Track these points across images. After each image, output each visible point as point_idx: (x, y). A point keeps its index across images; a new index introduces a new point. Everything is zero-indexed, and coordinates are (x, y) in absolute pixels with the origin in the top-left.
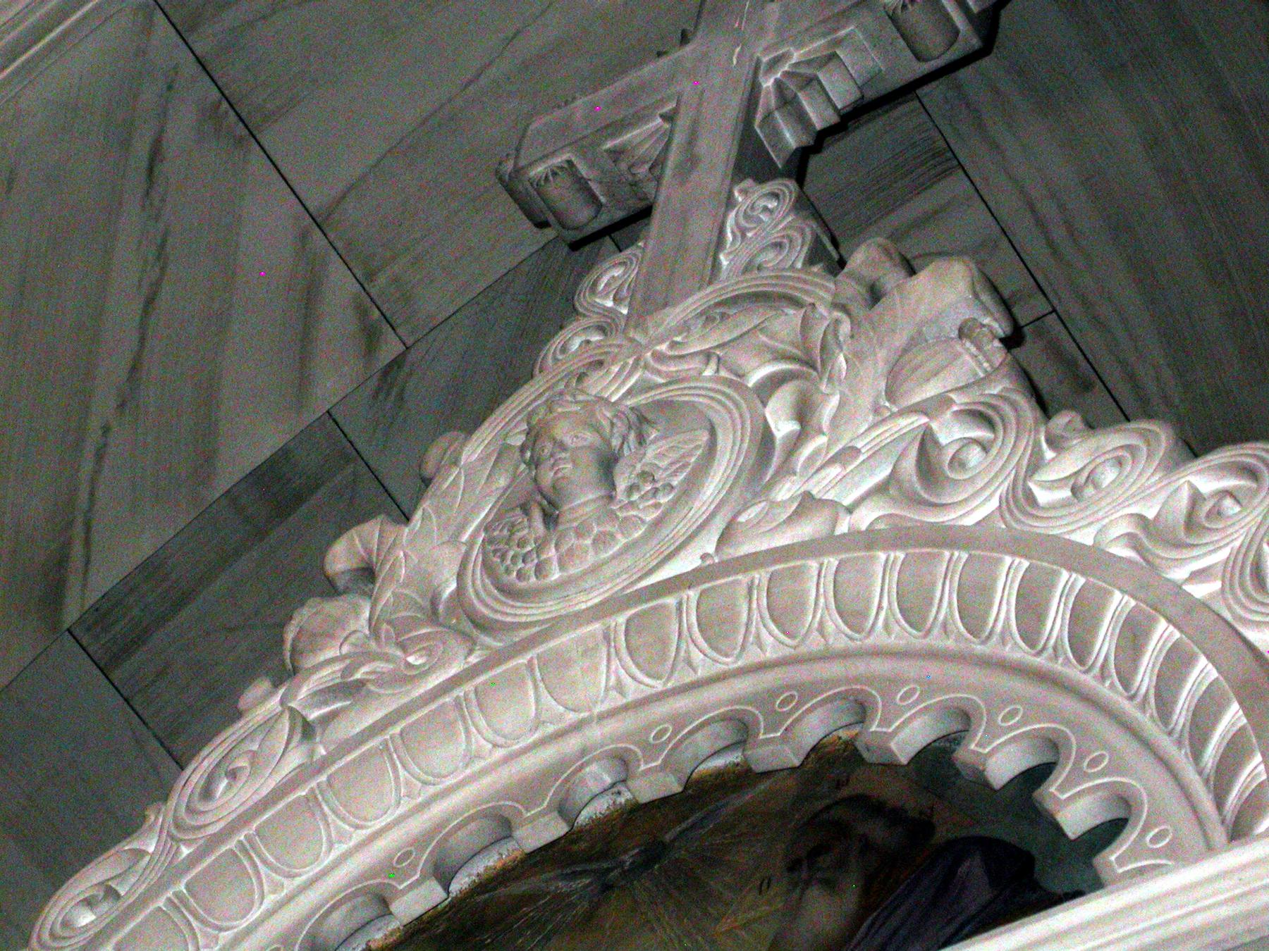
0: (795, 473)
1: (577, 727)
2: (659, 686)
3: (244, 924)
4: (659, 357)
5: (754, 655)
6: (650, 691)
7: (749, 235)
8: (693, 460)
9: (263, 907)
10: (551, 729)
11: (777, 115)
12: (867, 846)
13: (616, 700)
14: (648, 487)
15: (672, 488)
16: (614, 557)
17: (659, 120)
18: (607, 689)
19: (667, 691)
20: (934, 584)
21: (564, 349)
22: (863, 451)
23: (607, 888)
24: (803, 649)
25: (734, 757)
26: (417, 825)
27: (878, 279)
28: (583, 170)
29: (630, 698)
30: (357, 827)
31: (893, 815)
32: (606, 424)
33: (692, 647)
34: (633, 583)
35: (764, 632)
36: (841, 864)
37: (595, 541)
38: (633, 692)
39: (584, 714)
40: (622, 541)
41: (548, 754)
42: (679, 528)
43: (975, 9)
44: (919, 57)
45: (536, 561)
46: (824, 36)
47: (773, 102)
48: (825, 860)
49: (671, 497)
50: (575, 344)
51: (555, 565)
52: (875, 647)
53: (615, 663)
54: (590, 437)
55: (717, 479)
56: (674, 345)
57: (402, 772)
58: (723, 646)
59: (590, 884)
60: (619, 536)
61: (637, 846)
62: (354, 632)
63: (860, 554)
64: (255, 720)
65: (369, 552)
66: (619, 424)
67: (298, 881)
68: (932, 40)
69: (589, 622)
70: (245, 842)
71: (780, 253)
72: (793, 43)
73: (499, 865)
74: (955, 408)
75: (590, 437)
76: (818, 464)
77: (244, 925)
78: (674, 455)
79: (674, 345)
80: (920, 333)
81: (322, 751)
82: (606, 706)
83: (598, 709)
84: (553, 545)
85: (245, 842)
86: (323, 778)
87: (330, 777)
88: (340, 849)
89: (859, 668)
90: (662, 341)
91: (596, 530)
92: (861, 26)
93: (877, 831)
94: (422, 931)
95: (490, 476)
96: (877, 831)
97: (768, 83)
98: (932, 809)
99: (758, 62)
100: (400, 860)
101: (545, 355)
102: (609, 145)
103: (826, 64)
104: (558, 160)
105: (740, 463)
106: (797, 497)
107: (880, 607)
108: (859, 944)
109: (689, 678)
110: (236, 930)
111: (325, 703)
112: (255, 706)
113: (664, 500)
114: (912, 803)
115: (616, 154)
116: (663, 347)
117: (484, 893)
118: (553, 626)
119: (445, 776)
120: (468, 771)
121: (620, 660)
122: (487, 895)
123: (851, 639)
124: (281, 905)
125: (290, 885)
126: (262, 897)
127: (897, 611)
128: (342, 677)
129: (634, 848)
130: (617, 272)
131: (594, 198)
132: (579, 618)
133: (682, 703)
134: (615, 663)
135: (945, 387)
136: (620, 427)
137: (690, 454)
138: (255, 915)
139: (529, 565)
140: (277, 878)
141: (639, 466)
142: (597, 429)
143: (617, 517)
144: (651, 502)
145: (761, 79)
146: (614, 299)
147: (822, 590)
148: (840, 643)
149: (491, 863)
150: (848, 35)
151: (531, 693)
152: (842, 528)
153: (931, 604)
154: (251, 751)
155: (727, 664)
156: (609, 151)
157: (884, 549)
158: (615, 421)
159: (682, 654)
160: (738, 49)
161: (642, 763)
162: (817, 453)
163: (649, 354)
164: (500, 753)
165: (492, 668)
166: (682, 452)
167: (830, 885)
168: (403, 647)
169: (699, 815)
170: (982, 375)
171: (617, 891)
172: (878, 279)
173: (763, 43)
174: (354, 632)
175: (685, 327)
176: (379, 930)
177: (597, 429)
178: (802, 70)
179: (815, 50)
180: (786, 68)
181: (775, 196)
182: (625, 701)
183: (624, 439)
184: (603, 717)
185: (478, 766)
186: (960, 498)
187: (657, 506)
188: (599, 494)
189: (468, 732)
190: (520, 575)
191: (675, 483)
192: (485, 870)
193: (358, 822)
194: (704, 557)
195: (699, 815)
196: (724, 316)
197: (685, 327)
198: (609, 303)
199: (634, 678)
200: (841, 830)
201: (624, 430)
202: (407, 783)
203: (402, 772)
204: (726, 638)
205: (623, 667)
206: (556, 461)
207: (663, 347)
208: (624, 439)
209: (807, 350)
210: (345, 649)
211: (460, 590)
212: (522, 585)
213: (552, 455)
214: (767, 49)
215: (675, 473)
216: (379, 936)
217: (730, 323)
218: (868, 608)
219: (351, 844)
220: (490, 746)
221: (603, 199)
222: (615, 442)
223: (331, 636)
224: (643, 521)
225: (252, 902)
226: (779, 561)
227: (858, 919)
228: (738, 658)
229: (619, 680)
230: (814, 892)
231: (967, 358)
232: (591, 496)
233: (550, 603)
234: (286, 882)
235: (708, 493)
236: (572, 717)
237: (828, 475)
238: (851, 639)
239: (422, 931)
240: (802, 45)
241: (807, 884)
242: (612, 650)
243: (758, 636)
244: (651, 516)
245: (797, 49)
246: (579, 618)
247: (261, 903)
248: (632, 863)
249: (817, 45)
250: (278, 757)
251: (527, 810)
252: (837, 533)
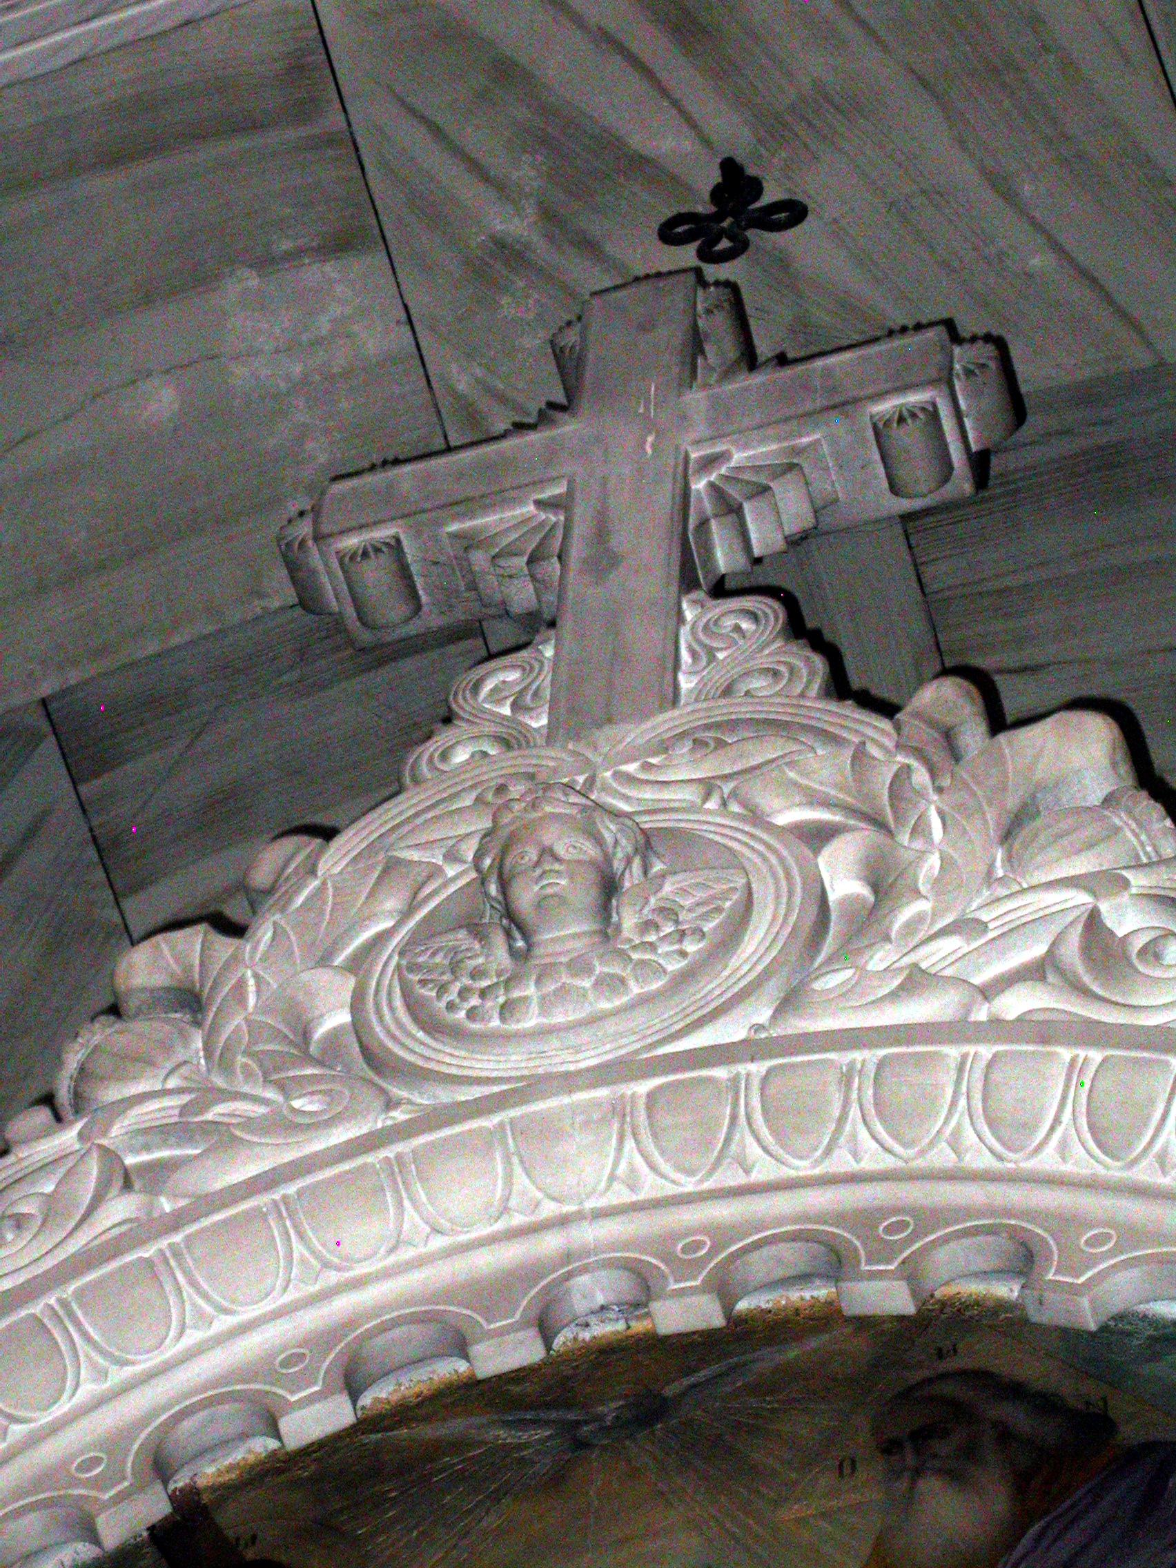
0: (887, 938)
1: (563, 1221)
2: (689, 1185)
3: (45, 1419)
4: (630, 779)
5: (842, 1162)
6: (672, 1190)
7: (721, 656)
8: (728, 904)
9: (75, 1400)
10: (518, 1220)
11: (714, 525)
12: (1005, 1435)
13: (621, 1195)
14: (668, 928)
15: (703, 935)
16: (616, 1012)
17: (530, 508)
18: (612, 1177)
19: (700, 1193)
20: (1151, 1101)
21: (445, 756)
22: (991, 926)
23: (581, 1445)
24: (920, 1163)
25: (821, 1292)
26: (311, 1320)
27: (953, 728)
28: (411, 551)
29: (641, 1196)
30: (227, 1311)
31: (1046, 1404)
32: (609, 839)
33: (750, 1140)
34: (653, 1046)
35: (863, 1134)
36: (969, 1452)
37: (596, 984)
38: (652, 1187)
39: (570, 1208)
40: (635, 989)
41: (512, 1254)
42: (713, 987)
43: (974, 447)
44: (895, 489)
45: (501, 1000)
46: (780, 440)
47: (708, 507)
48: (944, 1448)
49: (701, 945)
50: (461, 756)
51: (534, 1007)
52: (1032, 1171)
53: (630, 1144)
54: (590, 850)
55: (761, 933)
56: (647, 767)
57: (298, 1248)
58: (799, 1143)
59: (549, 1437)
60: (632, 983)
61: (621, 1397)
62: (185, 1062)
63: (1031, 1048)
64: (31, 1160)
65: (188, 969)
66: (624, 842)
67: (129, 1371)
68: (918, 472)
69: (592, 1086)
70: (58, 1308)
71: (776, 683)
72: (735, 443)
73: (395, 1398)
74: (1134, 891)
75: (590, 850)
76: (922, 935)
77: (43, 1421)
78: (701, 895)
79: (647, 767)
80: (1034, 797)
81: (166, 1205)
82: (601, 1203)
83: (591, 1204)
84: (534, 977)
85: (58, 1308)
86: (178, 1238)
87: (188, 1239)
88: (193, 1337)
89: (1014, 1196)
90: (628, 760)
91: (597, 972)
92: (834, 440)
93: (1019, 1417)
94: (280, 1471)
95: (371, 895)
96: (1019, 1417)
97: (699, 485)
98: (1105, 1400)
99: (686, 459)
100: (286, 1363)
101: (419, 757)
102: (454, 527)
103: (783, 473)
104: (915, 398)
105: (793, 919)
106: (901, 969)
107: (1057, 1121)
108: (1024, 1558)
109: (740, 1179)
110: (32, 1425)
111: (147, 1148)
112: (27, 1141)
113: (691, 947)
114: (1069, 1388)
115: (469, 542)
116: (632, 768)
117: (375, 1431)
118: (530, 1085)
119: (360, 1261)
120: (391, 1260)
121: (637, 1142)
122: (379, 1435)
123: (1000, 1158)
124: (99, 1402)
125: (117, 1376)
126: (77, 1386)
127: (1085, 1128)
128: (181, 1114)
129: (614, 1399)
130: (513, 676)
131: (414, 596)
132: (569, 1081)
133: (722, 1212)
134: (630, 1144)
135: (1101, 865)
136: (626, 847)
137: (724, 896)
138: (63, 1407)
139: (489, 1004)
140: (101, 1361)
141: (653, 900)
142: (598, 840)
143: (631, 959)
144: (676, 947)
145: (692, 479)
146: (514, 706)
147: (964, 1089)
148: (985, 1161)
149: (383, 1395)
150: (810, 445)
151: (500, 1168)
152: (981, 1014)
153: (1145, 1124)
154: (42, 1194)
155: (797, 1168)
156: (455, 536)
157: (1069, 1044)
158: (619, 836)
159: (733, 1147)
160: (650, 439)
161: (671, 1280)
162: (919, 919)
163: (608, 774)
164: (438, 1243)
165: (430, 1129)
166: (712, 892)
167: (956, 1476)
168: (282, 1086)
169: (715, 1368)
170: (1145, 860)
171: (597, 1452)
172: (953, 728)
173: (692, 436)
174: (185, 1062)
175: (664, 747)
176: (213, 1461)
177: (598, 840)
178: (746, 476)
179: (767, 455)
180: (723, 471)
181: (753, 616)
182: (634, 1198)
183: (629, 861)
184: (601, 1214)
185: (406, 1254)
186: (1160, 1001)
187: (683, 954)
188: (594, 927)
189: (400, 1205)
190: (472, 1014)
191: (708, 927)
192: (372, 1404)
193: (226, 1304)
194: (759, 1028)
195: (715, 1368)
196: (721, 744)
197: (664, 747)
198: (506, 710)
199: (652, 1167)
200: (960, 1411)
201: (630, 849)
202: (303, 1261)
203: (298, 1248)
204: (805, 1132)
205: (640, 1151)
206: (544, 872)
207: (632, 768)
208: (629, 861)
209: (870, 798)
210: (172, 1083)
211: (358, 1026)
212: (476, 1026)
213: (537, 864)
214: (698, 442)
215: (705, 917)
216: (210, 1470)
217: (731, 752)
218: (1038, 1121)
219: (211, 1332)
220: (428, 1230)
221: (424, 599)
222: (618, 865)
223: (151, 1063)
224: (665, 971)
225: (61, 1391)
226: (897, 1042)
227: (1016, 1528)
228: (817, 1163)
229: (633, 1170)
230: (931, 1485)
231: (1129, 834)
232: (574, 930)
233: (514, 1058)
234: (114, 1369)
235: (750, 949)
236: (549, 1209)
237: (938, 950)
238: (1000, 1158)
239: (280, 1471)
240: (745, 447)
241: (918, 1472)
242: (628, 1128)
243: (853, 1137)
244: (674, 966)
245: (738, 450)
246: (569, 1081)
247: (73, 1395)
248: (617, 1417)
249: (765, 450)
250: (82, 1210)
251: (869, 1262)
252: (972, 1018)
